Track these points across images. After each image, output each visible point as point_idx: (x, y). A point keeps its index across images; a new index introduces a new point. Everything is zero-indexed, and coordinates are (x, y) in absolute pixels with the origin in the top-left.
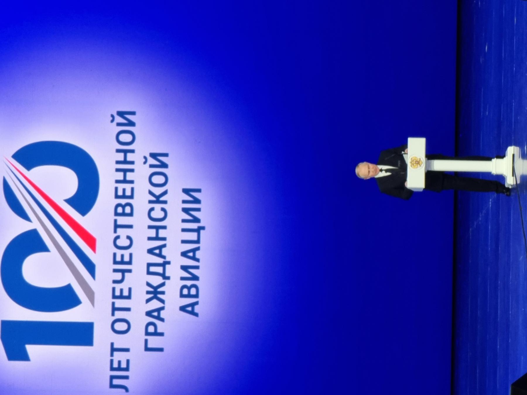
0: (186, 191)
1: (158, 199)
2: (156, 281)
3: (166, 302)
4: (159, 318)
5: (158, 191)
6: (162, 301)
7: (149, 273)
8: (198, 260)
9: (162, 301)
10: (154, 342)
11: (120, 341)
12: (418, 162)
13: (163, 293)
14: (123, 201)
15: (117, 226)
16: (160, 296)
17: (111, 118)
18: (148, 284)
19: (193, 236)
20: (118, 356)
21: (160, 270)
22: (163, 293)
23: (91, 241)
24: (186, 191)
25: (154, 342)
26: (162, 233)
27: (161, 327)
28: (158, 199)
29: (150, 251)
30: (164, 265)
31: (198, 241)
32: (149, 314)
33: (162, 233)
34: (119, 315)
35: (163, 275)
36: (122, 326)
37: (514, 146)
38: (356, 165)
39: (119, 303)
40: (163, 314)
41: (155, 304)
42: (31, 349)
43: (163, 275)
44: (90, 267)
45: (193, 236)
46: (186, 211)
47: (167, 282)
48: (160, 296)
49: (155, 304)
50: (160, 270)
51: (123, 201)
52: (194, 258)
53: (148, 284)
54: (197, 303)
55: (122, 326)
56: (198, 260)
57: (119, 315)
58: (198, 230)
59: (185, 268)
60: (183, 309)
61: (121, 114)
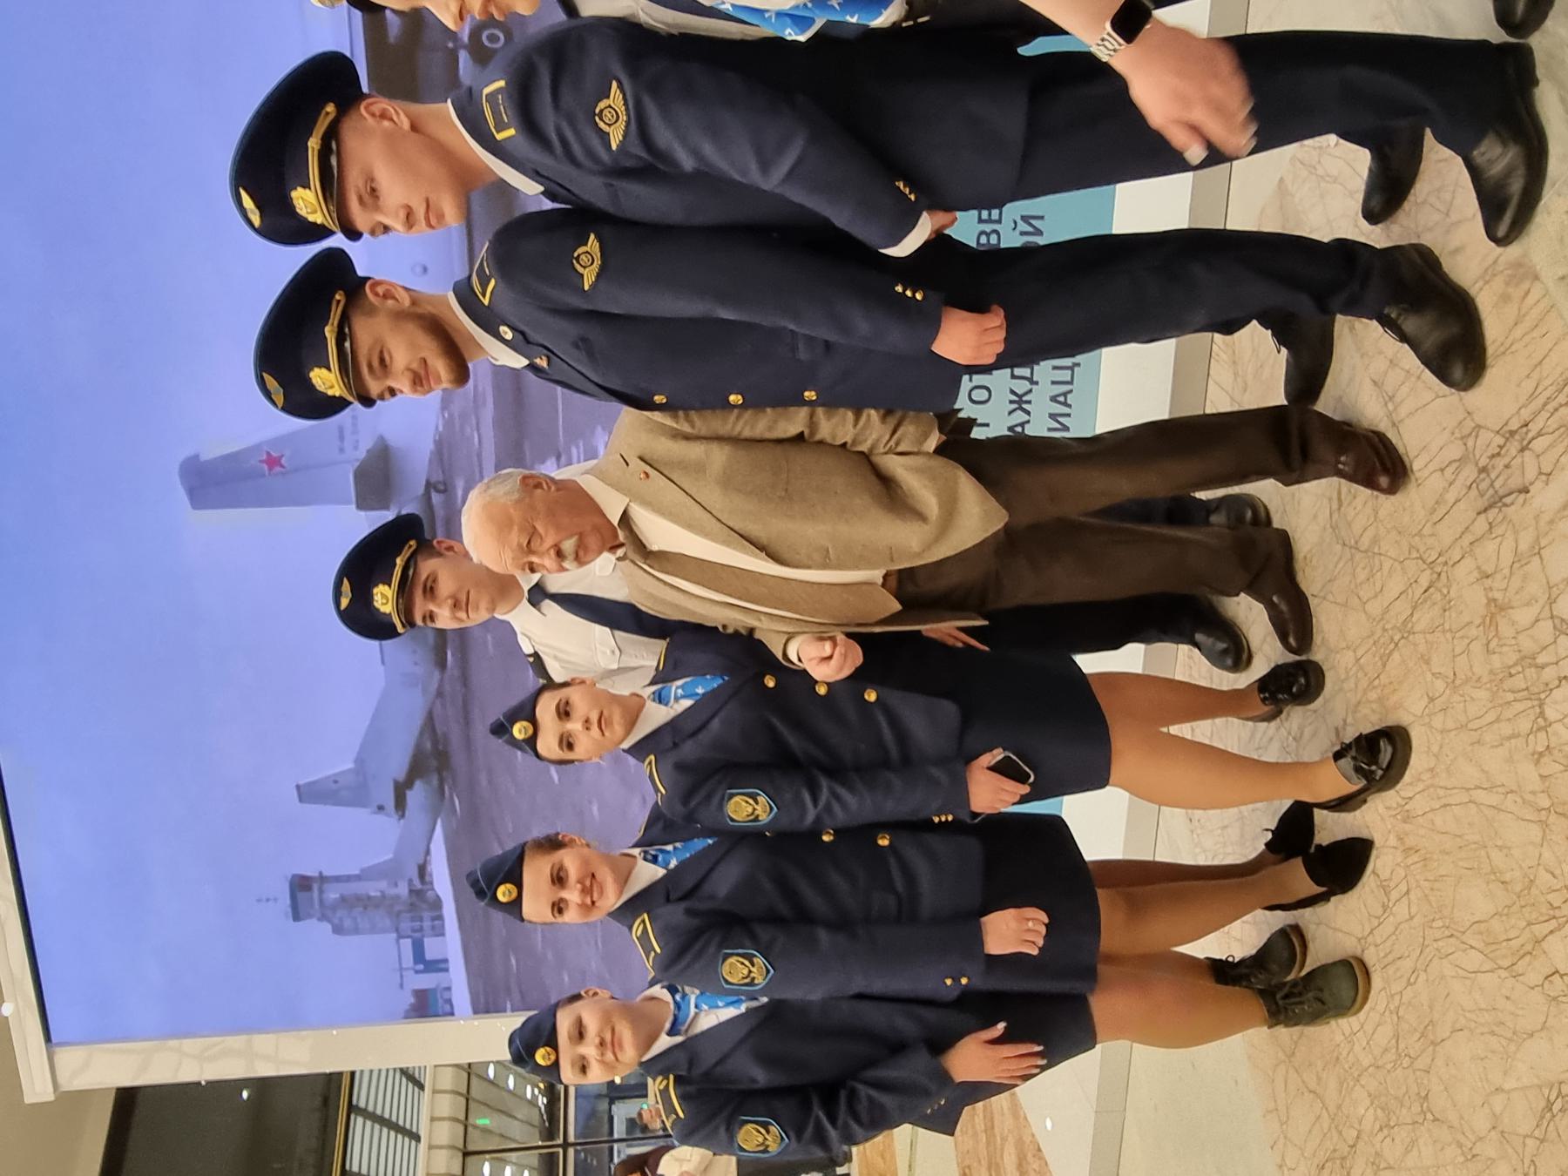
3: (1032, 414)
6: (1028, 413)
8: (1070, 406)
9: (1028, 413)
13: (1029, 402)
14: (988, 228)
16: (1024, 406)
17: (1013, 225)
18: (1013, 392)
19: (1066, 376)
22: (1029, 402)
31: (1071, 383)
35: (1031, 380)
38: (772, 688)
43: (1031, 380)
47: (1034, 387)
48: (1024, 406)
51: (988, 228)
52: (1065, 404)
53: (1013, 392)
54: (1071, 391)
56: (1070, 406)
61: (1025, 219)
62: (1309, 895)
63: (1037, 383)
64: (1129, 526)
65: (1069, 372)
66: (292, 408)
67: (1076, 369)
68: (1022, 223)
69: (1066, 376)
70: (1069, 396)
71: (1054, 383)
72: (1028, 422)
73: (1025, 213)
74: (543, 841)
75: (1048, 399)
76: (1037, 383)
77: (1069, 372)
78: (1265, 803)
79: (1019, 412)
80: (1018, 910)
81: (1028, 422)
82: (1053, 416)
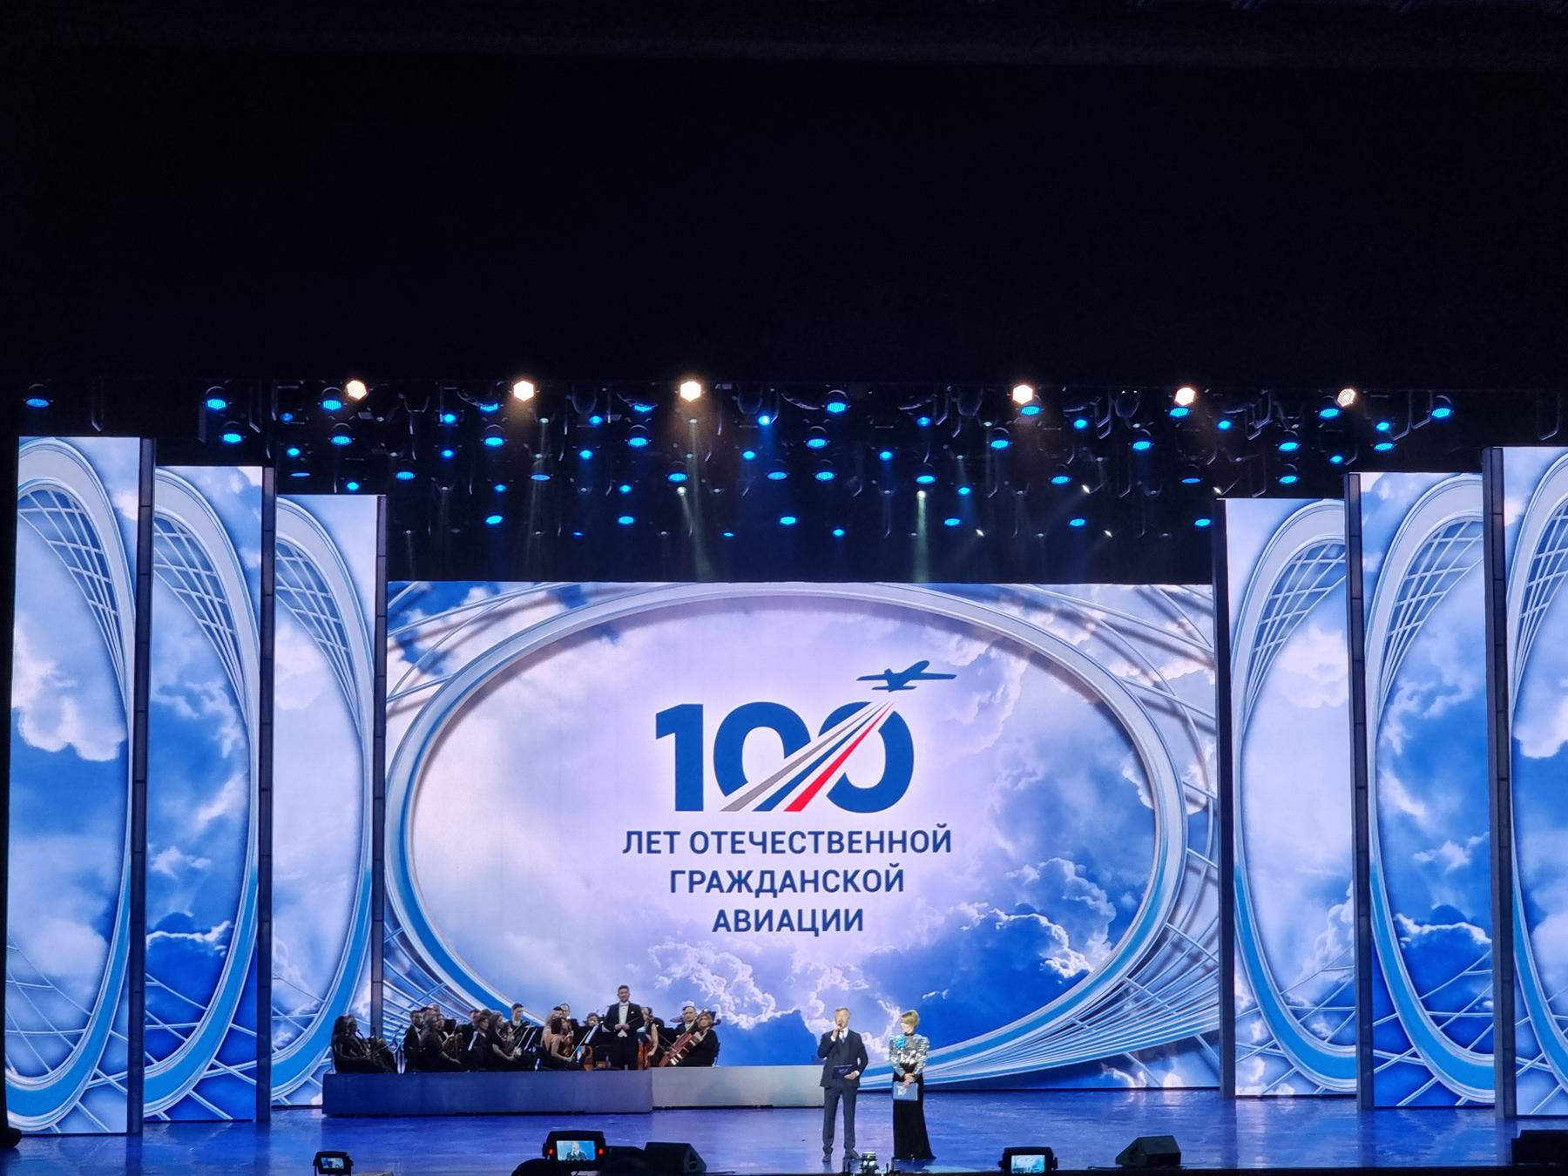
3: (728, 894)
6: (730, 890)
8: (779, 929)
9: (730, 890)
14: (845, 841)
15: (816, 834)
16: (736, 886)
18: (749, 873)
19: (807, 923)
20: (665, 840)
24: (859, 914)
29: (788, 875)
31: (801, 929)
39: (726, 840)
46: (837, 914)
47: (753, 894)
48: (736, 886)
51: (845, 841)
52: (781, 925)
53: (749, 873)
56: (779, 929)
57: (713, 840)
60: (722, 914)
62: (430, 956)
63: (757, 896)
64: (1335, 994)
65: (809, 926)
66: (345, 1153)
67: (813, 933)
68: (943, 833)
69: (807, 923)
70: (788, 928)
71: (800, 912)
72: (722, 891)
73: (952, 835)
74: (336, 1036)
75: (786, 908)
76: (757, 896)
77: (809, 926)
78: (369, 1024)
79: (730, 881)
80: (1373, 1166)
81: (722, 891)
82: (769, 914)
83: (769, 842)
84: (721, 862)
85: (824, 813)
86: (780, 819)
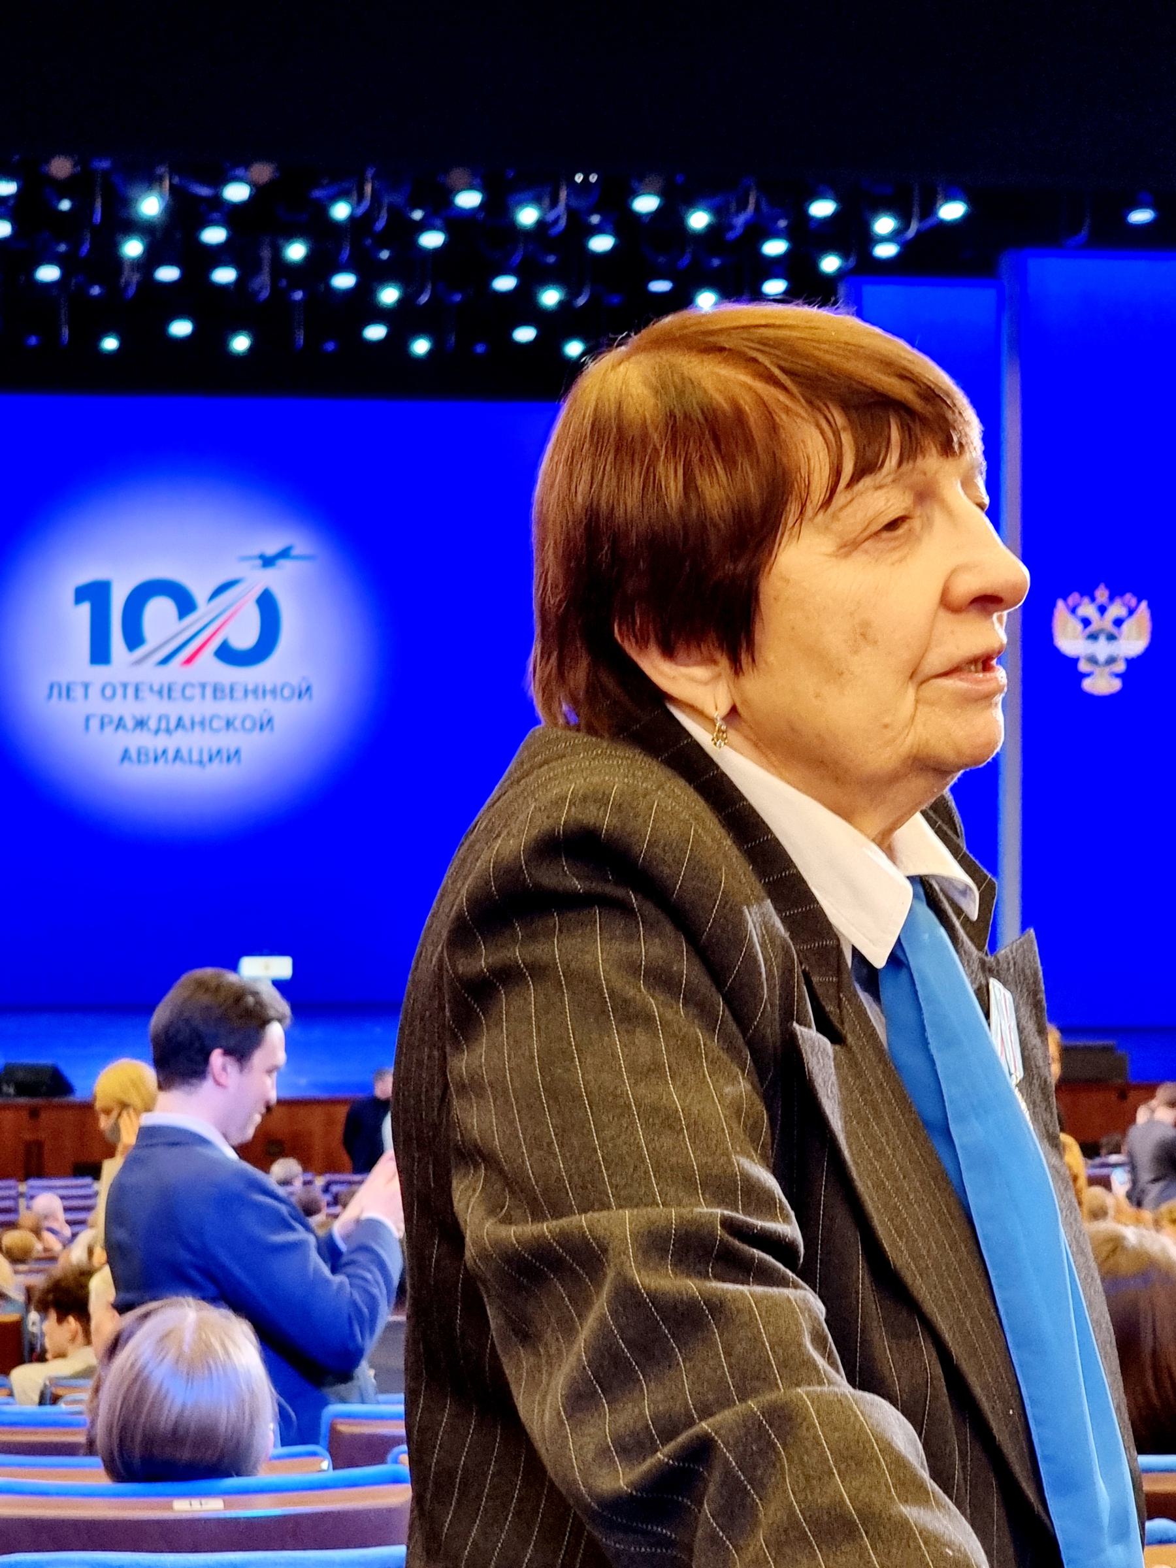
0: (237, 752)
1: (229, 724)
2: (153, 724)
4: (118, 727)
5: (237, 723)
7: (160, 719)
10: (94, 724)
11: (94, 691)
12: (267, 968)
15: (203, 686)
19: (195, 757)
21: (163, 725)
23: (189, 661)
24: (237, 752)
25: (94, 724)
26: (197, 728)
27: (109, 730)
28: (229, 724)
29: (180, 720)
30: (168, 731)
32: (121, 719)
33: (197, 728)
34: (120, 692)
35: (157, 732)
36: (108, 692)
37: (703, 525)
40: (121, 731)
41: (130, 723)
42: (85, 608)
43: (157, 732)
44: (165, 661)
45: (195, 757)
49: (130, 723)
50: (163, 725)
55: (108, 692)
57: (120, 692)
58: (201, 762)
59: (164, 752)
83: (166, 692)
84: (128, 709)
85: (209, 667)
86: (175, 672)
